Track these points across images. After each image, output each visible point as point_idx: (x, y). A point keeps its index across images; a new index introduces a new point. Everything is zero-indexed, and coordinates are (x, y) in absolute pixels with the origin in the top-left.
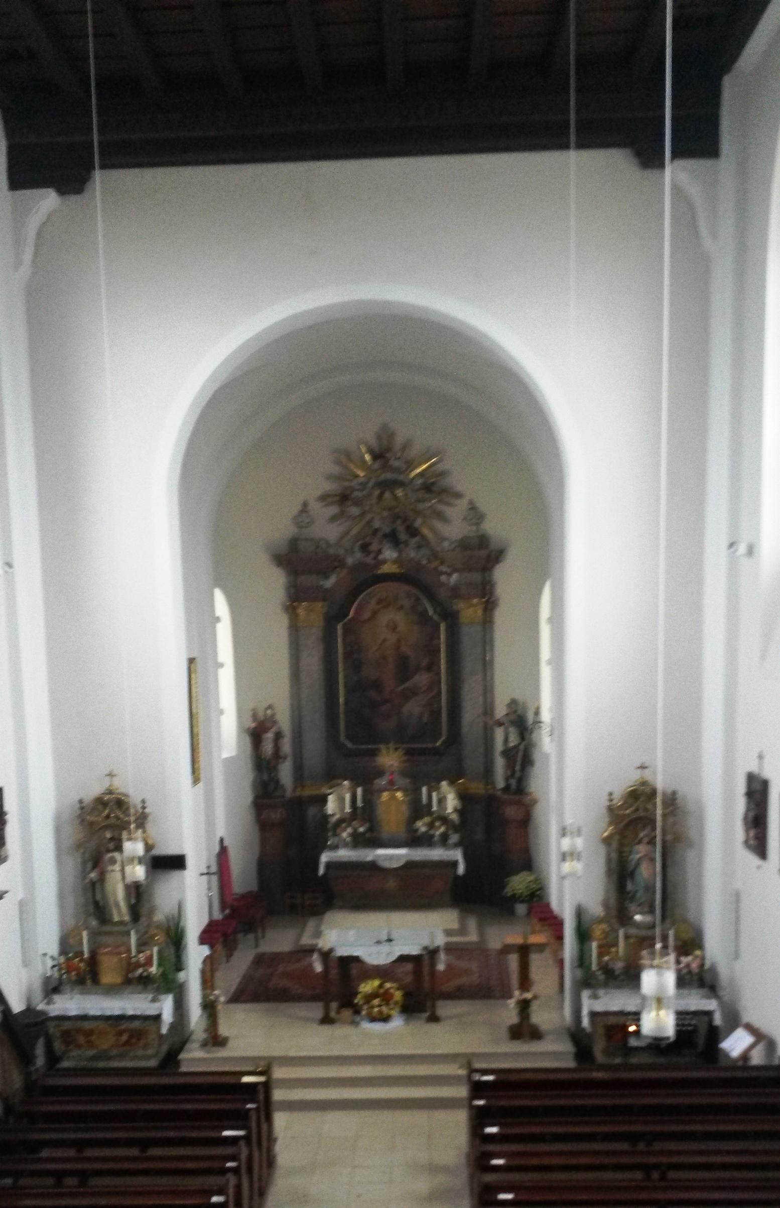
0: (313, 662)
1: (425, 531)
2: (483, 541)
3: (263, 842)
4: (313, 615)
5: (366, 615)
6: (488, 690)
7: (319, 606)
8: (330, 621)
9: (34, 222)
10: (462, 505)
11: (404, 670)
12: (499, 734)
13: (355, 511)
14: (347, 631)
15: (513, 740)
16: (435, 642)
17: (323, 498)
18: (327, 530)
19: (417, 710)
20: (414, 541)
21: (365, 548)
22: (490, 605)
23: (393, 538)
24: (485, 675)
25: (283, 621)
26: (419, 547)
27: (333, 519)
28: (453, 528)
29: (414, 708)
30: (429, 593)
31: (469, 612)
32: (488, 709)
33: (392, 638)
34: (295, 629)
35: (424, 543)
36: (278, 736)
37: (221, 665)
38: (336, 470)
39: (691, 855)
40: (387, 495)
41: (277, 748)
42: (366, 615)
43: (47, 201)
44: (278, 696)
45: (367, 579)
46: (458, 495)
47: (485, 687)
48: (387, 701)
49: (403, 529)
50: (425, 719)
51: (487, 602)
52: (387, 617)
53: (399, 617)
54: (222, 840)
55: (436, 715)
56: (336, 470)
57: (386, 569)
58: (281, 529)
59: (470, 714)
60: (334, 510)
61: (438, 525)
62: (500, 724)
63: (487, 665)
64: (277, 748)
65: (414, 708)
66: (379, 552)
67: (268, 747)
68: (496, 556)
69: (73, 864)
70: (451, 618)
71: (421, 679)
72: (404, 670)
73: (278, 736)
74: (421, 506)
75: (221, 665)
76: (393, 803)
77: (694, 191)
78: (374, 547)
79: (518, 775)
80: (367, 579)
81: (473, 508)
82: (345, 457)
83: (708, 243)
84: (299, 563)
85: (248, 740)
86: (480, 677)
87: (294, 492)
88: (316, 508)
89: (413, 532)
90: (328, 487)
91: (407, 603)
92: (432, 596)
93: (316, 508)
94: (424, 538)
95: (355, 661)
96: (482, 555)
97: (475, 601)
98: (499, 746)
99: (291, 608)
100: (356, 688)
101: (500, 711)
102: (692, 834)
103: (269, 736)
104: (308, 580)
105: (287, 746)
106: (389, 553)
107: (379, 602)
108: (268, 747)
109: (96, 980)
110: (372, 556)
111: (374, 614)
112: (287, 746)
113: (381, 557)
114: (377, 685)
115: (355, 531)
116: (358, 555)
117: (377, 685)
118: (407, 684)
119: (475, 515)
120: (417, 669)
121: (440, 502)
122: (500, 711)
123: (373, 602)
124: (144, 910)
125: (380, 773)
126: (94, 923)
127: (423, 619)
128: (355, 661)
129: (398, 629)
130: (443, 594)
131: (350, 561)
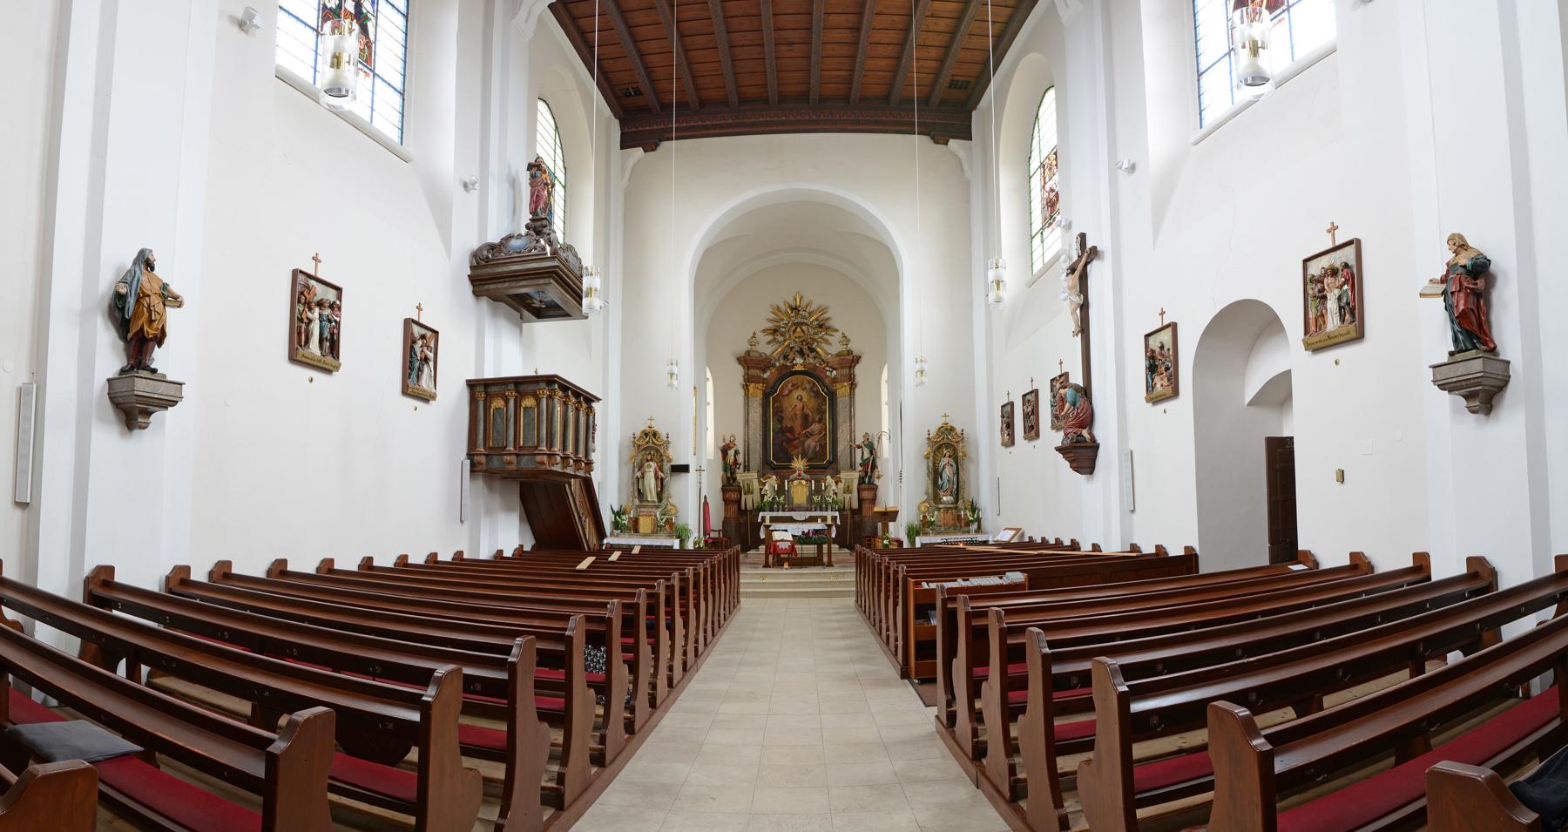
2: (850, 352)
3: (726, 511)
4: (757, 392)
7: (760, 386)
8: (766, 396)
9: (631, 162)
10: (838, 335)
12: (859, 452)
13: (781, 339)
15: (866, 455)
18: (766, 348)
21: (786, 357)
22: (853, 386)
23: (801, 353)
28: (831, 347)
29: (811, 443)
30: (820, 380)
31: (842, 390)
32: (852, 439)
33: (800, 405)
34: (747, 395)
35: (818, 356)
36: (737, 453)
38: (772, 316)
39: (972, 467)
43: (638, 152)
45: (787, 372)
49: (806, 349)
52: (796, 394)
53: (804, 394)
56: (772, 316)
58: (743, 347)
59: (842, 446)
63: (851, 417)
65: (811, 443)
67: (731, 458)
68: (857, 360)
69: (628, 470)
70: (833, 395)
71: (816, 427)
76: (800, 491)
77: (961, 153)
80: (787, 372)
83: (968, 173)
84: (750, 363)
87: (750, 326)
89: (812, 350)
90: (770, 325)
92: (820, 380)
95: (780, 419)
96: (850, 361)
98: (859, 460)
99: (746, 387)
100: (781, 431)
101: (859, 441)
102: (973, 455)
103: (731, 452)
104: (752, 372)
105: (740, 459)
106: (799, 360)
108: (731, 458)
109: (636, 531)
112: (740, 459)
114: (791, 430)
117: (791, 430)
122: (859, 441)
124: (665, 495)
126: (637, 502)
127: (817, 394)
128: (780, 419)
130: (827, 381)
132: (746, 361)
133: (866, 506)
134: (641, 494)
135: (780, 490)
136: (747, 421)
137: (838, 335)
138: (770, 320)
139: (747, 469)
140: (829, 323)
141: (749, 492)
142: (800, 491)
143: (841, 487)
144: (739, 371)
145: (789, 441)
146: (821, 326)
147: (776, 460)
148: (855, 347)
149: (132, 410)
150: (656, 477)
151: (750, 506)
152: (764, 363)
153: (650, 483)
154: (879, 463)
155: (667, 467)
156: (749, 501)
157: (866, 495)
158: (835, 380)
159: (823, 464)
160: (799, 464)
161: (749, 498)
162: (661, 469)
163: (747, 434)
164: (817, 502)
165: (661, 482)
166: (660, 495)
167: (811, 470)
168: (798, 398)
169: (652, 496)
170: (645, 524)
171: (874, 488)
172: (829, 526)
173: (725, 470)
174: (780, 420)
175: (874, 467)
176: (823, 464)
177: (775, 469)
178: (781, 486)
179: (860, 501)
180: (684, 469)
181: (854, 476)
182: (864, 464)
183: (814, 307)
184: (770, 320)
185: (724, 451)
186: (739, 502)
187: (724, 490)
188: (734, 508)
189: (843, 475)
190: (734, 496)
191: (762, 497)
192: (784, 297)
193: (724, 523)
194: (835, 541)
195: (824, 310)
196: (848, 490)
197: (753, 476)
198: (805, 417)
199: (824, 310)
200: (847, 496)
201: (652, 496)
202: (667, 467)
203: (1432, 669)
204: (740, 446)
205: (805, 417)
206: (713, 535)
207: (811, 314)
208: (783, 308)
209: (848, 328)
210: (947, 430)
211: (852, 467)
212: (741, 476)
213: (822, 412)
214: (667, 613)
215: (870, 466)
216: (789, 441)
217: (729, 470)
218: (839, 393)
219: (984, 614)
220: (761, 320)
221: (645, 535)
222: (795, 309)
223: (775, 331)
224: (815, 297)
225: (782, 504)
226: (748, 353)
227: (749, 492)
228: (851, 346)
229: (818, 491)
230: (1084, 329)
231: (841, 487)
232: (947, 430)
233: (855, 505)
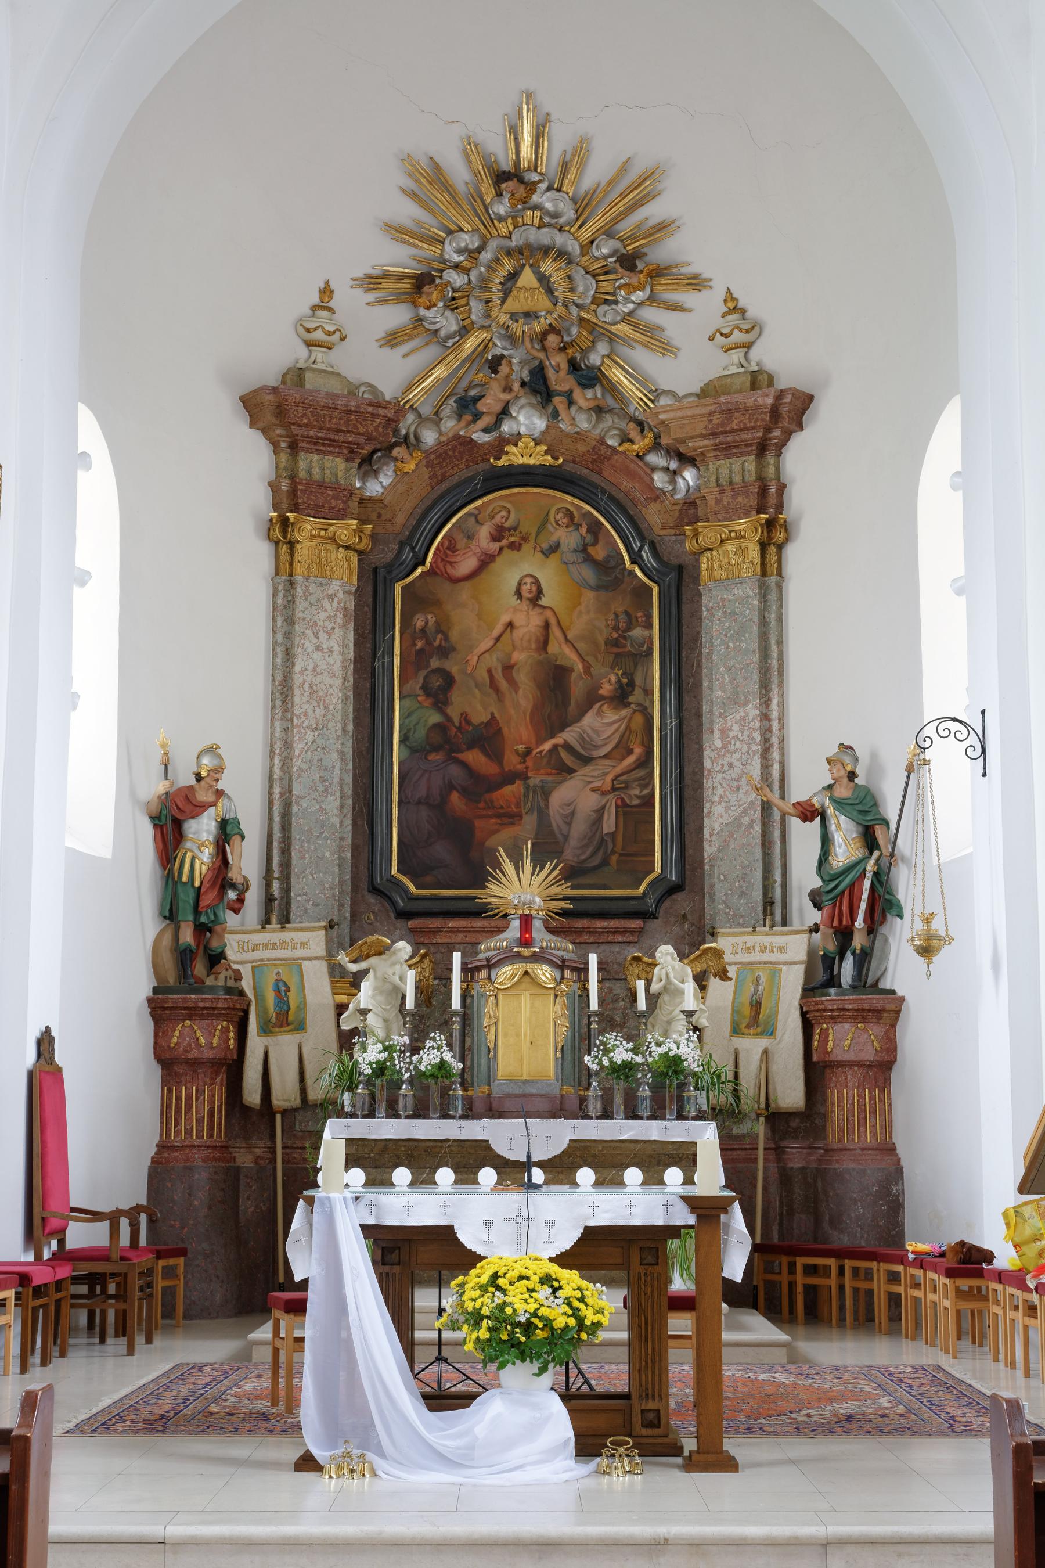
0: (328, 657)
1: (617, 375)
2: (758, 379)
3: (168, 1110)
5: (466, 564)
6: (771, 743)
7: (346, 529)
8: (374, 584)
10: (706, 307)
11: (557, 696)
12: (804, 839)
13: (448, 323)
14: (415, 600)
15: (846, 849)
16: (637, 632)
17: (372, 282)
18: (378, 361)
19: (589, 802)
20: (584, 398)
21: (467, 406)
22: (774, 535)
23: (539, 387)
24: (767, 703)
25: (261, 555)
26: (599, 411)
27: (392, 339)
28: (675, 362)
29: (579, 797)
30: (618, 507)
31: (725, 558)
32: (773, 775)
33: (528, 623)
34: (285, 572)
36: (227, 832)
37: (83, 578)
38: (408, 212)
40: (527, 278)
41: (222, 861)
42: (466, 564)
44: (233, 733)
46: (696, 283)
47: (766, 732)
48: (509, 778)
50: (609, 824)
51: (770, 524)
52: (513, 572)
53: (548, 574)
54: (45, 1042)
55: (635, 815)
56: (408, 212)
57: (516, 456)
58: (271, 352)
59: (726, 809)
60: (399, 315)
61: (644, 358)
62: (808, 812)
63: (770, 674)
64: (222, 861)
66: (505, 412)
68: (790, 411)
70: (680, 583)
71: (601, 725)
72: (557, 696)
73: (227, 832)
74: (606, 315)
75: (83, 578)
76: (525, 1023)
78: (490, 404)
79: (858, 941)
80: (475, 475)
81: (733, 307)
82: (429, 180)
84: (307, 425)
85: (147, 831)
86: (753, 711)
88: (350, 301)
89: (589, 377)
90: (400, 258)
91: (569, 539)
93: (350, 301)
94: (612, 389)
96: (764, 418)
97: (741, 524)
98: (805, 876)
99: (281, 532)
100: (444, 741)
101: (808, 779)
103: (202, 829)
104: (314, 465)
106: (528, 420)
107: (498, 534)
110: (485, 421)
111: (486, 561)
112: (248, 861)
113: (506, 427)
114: (488, 737)
115: (440, 372)
116: (449, 425)
118: (569, 736)
119: (741, 325)
120: (592, 699)
121: (652, 300)
122: (808, 779)
123: (484, 532)
125: (495, 918)
127: (609, 575)
129: (544, 601)
130: (653, 516)
131: (429, 437)
132: (286, 412)
133: (845, 1095)
135: (427, 1015)
136: (283, 689)
137: (706, 307)
138: (398, 232)
139: (278, 910)
140: (663, 252)
141: (285, 1019)
142: (525, 1023)
143: (718, 1004)
144: (249, 464)
145: (479, 787)
146: (628, 262)
147: (418, 872)
148: (782, 356)
151: (285, 1092)
152: (367, 430)
154: (906, 887)
156: (278, 1061)
157: (844, 1041)
158: (690, 510)
159: (638, 891)
160: (522, 887)
161: (283, 1049)
163: (281, 749)
164: (618, 1088)
167: (575, 917)
168: (521, 594)
171: (884, 1011)
172: (709, 1211)
173: (170, 914)
174: (439, 690)
175: (883, 906)
176: (638, 891)
177: (407, 914)
178: (432, 992)
179: (816, 1071)
181: (781, 956)
182: (836, 894)
183: (596, 173)
184: (398, 232)
185: (169, 823)
186: (233, 1068)
187: (162, 1009)
188: (210, 1095)
189: (729, 944)
190: (207, 1038)
191: (347, 1040)
192: (463, 118)
193: (159, 1172)
194: (740, 1296)
195: (643, 187)
196: (753, 1018)
197: (306, 944)
198: (555, 680)
199: (643, 187)
200: (752, 1047)
204: (246, 798)
205: (555, 680)
206: (80, 1236)
207: (583, 206)
208: (460, 174)
209: (756, 264)
211: (773, 910)
212: (247, 945)
213: (628, 657)
215: (861, 906)
216: (479, 787)
217: (193, 915)
218: (711, 566)
219: (869, 1275)
220: (359, 230)
222: (508, 178)
223: (421, 282)
224: (604, 117)
225: (435, 1109)
226: (297, 375)
227: (285, 1019)
228: (768, 354)
229: (623, 1016)
230: (903, 802)
231: (718, 1004)
233: (791, 1093)
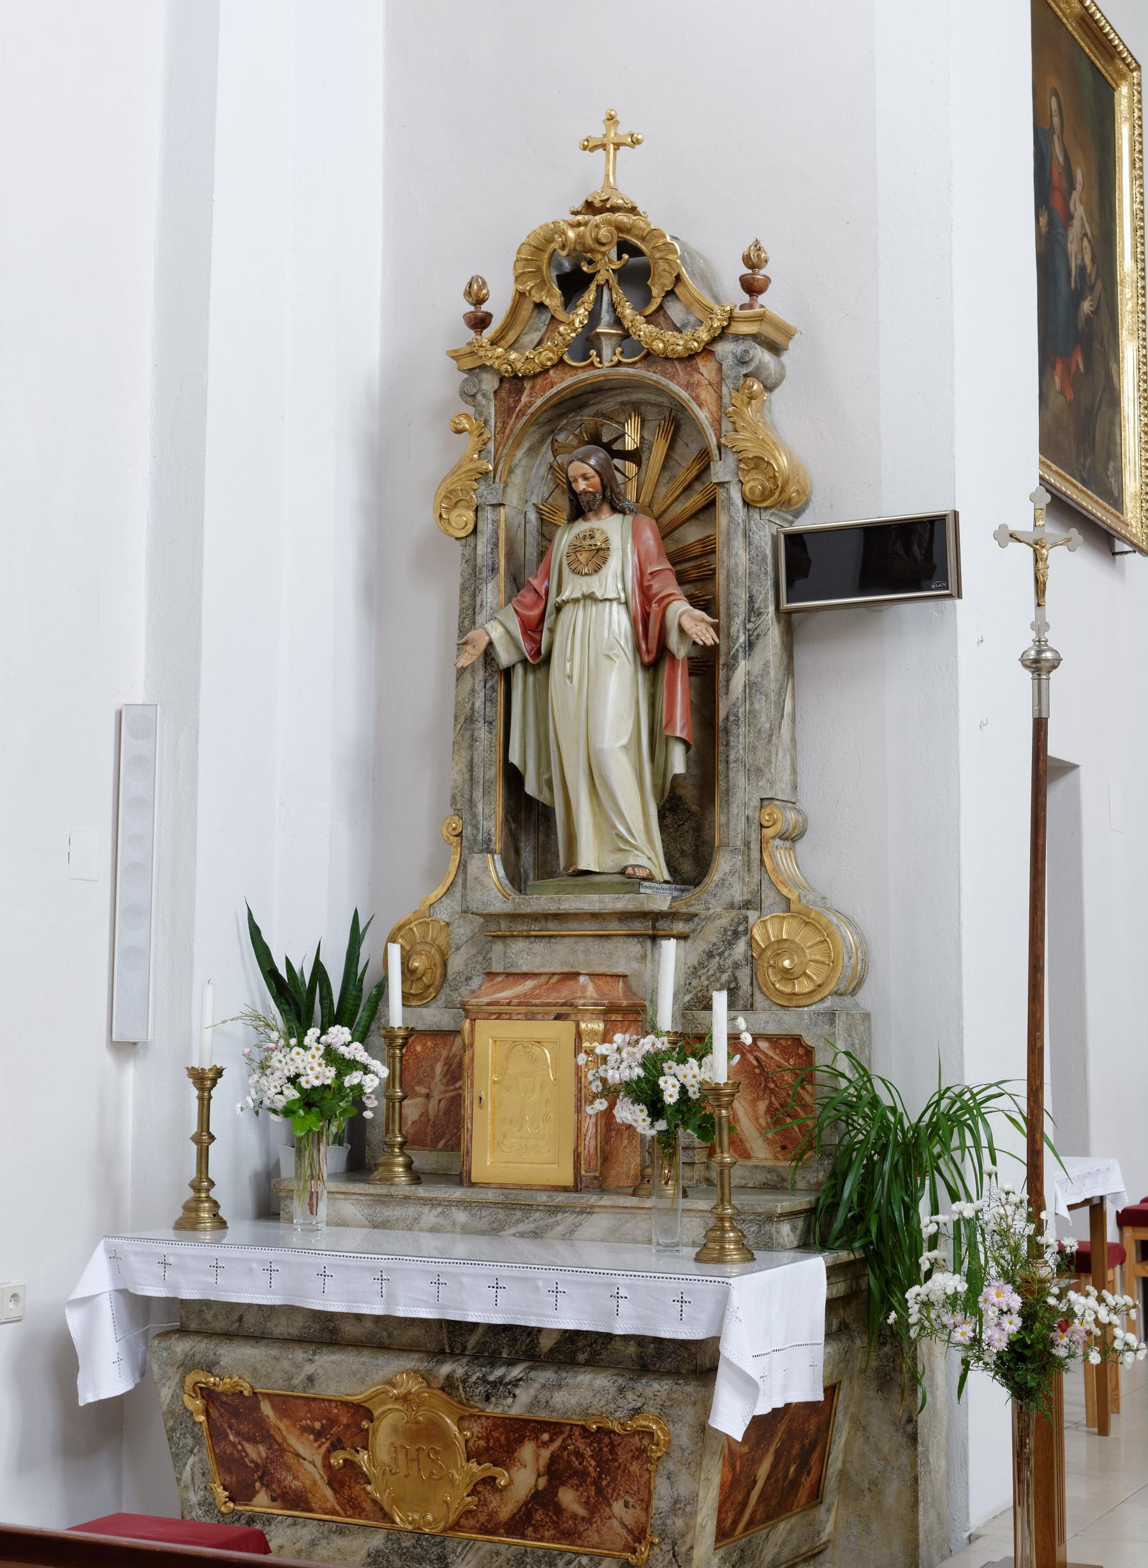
69: (430, 609)
124: (734, 817)
134: (530, 821)
149: (636, 142)
150: (653, 657)
153: (603, 704)
155: (747, 551)
162: (697, 573)
165: (693, 687)
166: (688, 816)
169: (615, 825)
170: (527, 1096)
180: (907, 558)
201: (615, 825)
202: (747, 551)
203: (1129, 60)
210: (602, 266)
214: (1133, 179)
221: (518, 1209)
232: (602, 266)
